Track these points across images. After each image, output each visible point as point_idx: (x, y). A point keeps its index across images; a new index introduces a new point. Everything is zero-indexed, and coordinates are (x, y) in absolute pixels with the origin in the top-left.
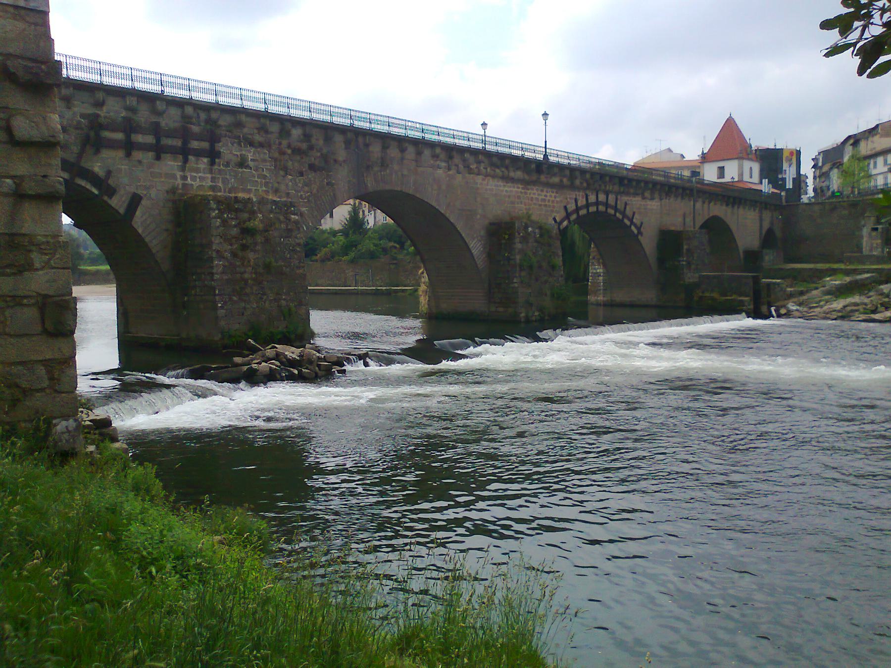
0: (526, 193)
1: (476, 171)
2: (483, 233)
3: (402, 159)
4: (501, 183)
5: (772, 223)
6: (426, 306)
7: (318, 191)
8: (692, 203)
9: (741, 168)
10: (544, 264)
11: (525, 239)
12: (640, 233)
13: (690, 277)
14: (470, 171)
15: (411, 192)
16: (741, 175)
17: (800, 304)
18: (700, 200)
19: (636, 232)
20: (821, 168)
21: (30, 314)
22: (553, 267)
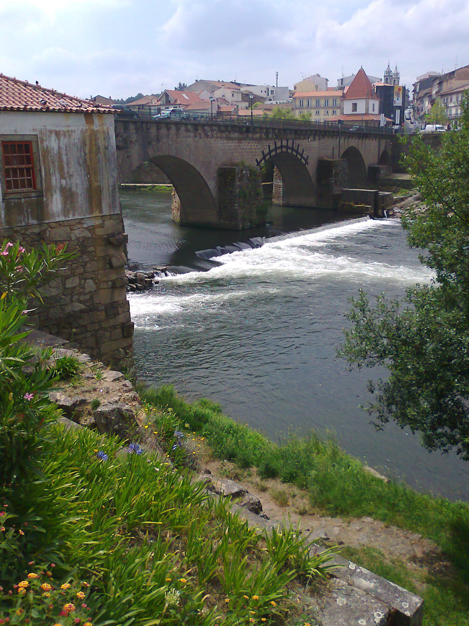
0: (240, 146)
1: (211, 136)
2: (215, 175)
3: (168, 134)
4: (225, 141)
5: (386, 147)
6: (179, 218)
7: (122, 162)
8: (338, 139)
9: (367, 105)
10: (252, 193)
11: (241, 179)
12: (307, 163)
13: (336, 191)
14: (207, 136)
15: (174, 155)
16: (367, 109)
17: (401, 208)
18: (343, 138)
19: (304, 162)
20: (418, 93)
21: (119, 331)
22: (258, 194)
